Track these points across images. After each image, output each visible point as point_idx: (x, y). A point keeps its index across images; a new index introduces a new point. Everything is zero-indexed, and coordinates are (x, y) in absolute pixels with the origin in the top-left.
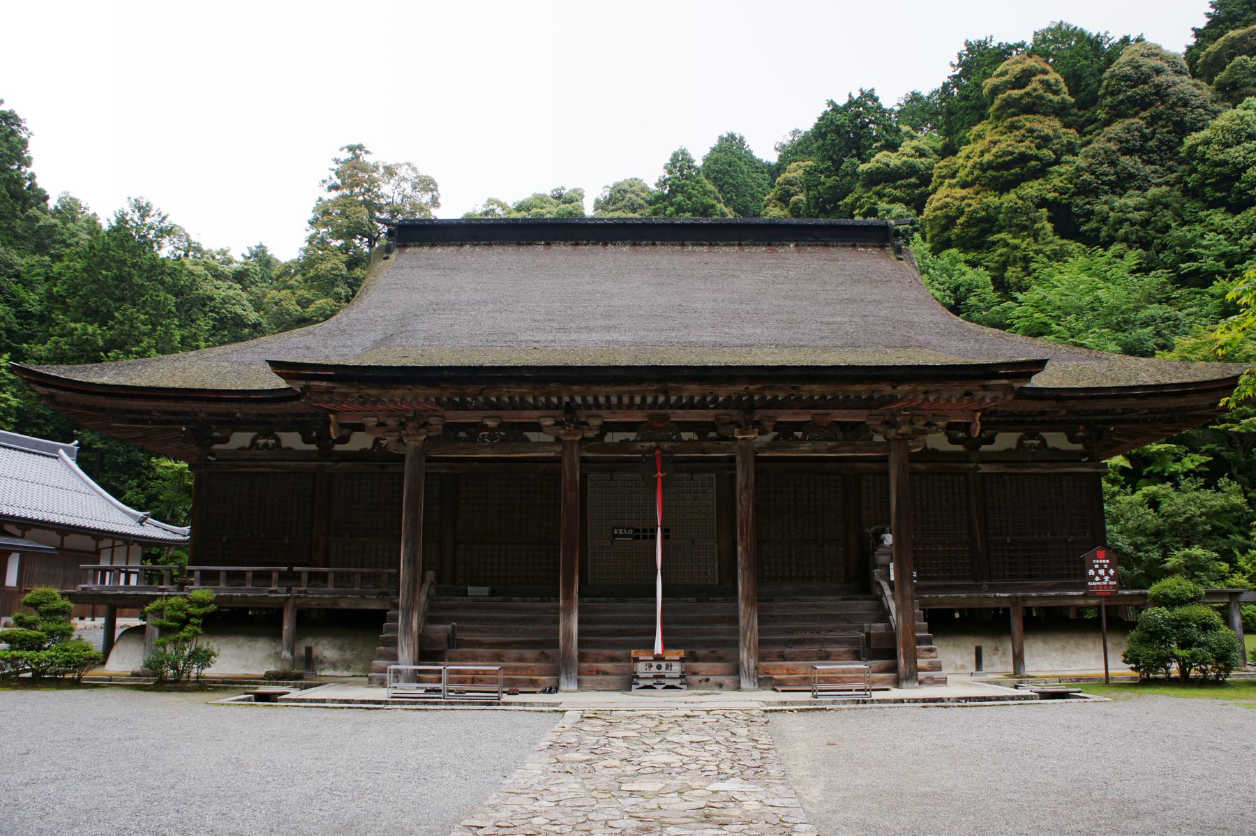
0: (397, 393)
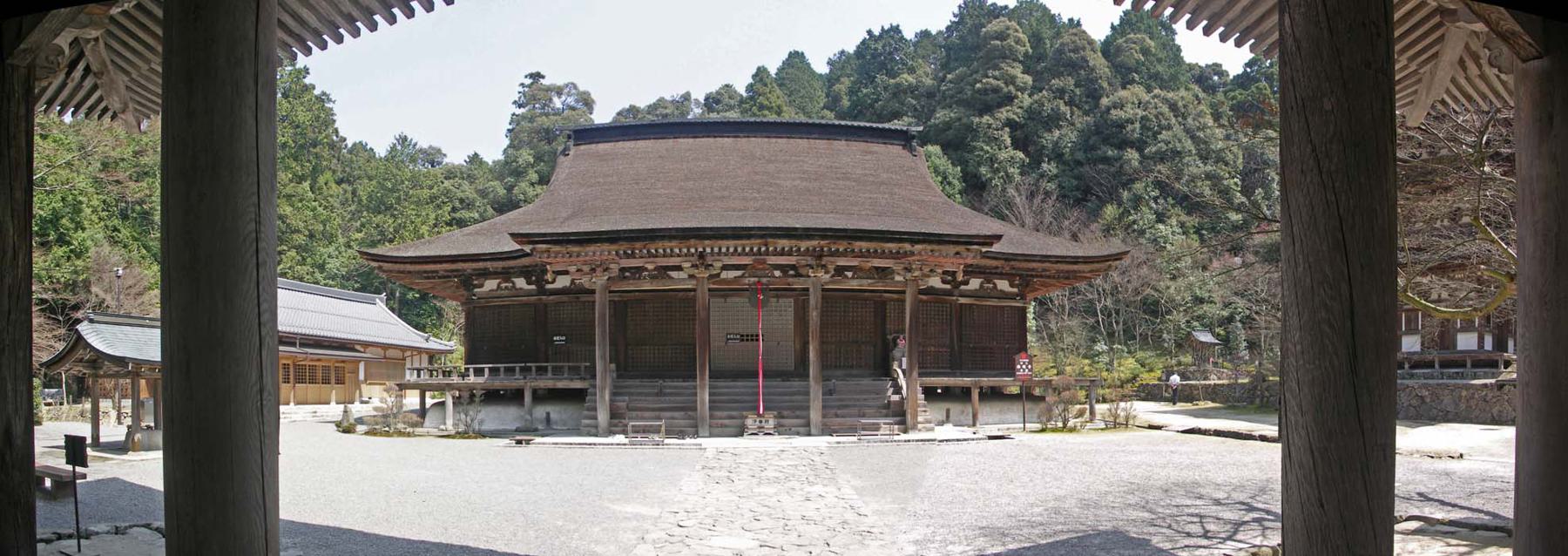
0: (591, 248)
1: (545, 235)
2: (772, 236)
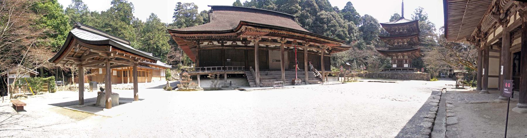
1: (253, 23)
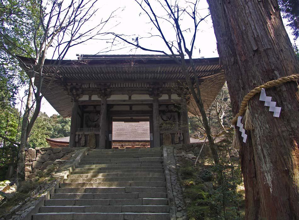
2: (135, 142)
